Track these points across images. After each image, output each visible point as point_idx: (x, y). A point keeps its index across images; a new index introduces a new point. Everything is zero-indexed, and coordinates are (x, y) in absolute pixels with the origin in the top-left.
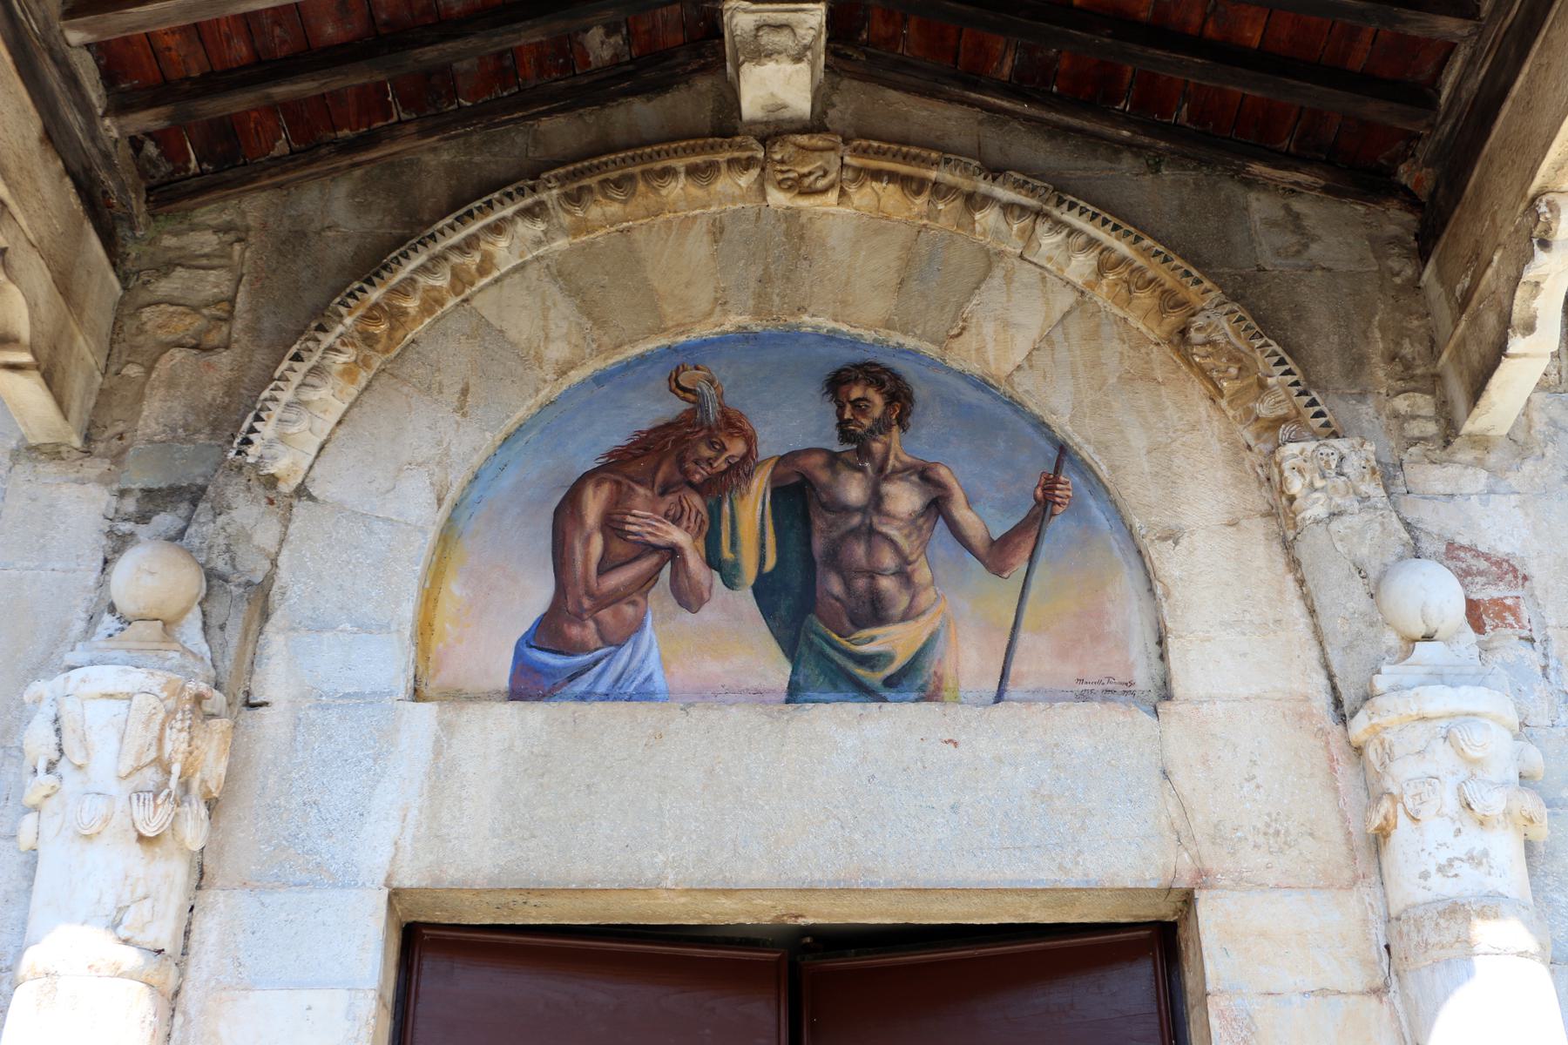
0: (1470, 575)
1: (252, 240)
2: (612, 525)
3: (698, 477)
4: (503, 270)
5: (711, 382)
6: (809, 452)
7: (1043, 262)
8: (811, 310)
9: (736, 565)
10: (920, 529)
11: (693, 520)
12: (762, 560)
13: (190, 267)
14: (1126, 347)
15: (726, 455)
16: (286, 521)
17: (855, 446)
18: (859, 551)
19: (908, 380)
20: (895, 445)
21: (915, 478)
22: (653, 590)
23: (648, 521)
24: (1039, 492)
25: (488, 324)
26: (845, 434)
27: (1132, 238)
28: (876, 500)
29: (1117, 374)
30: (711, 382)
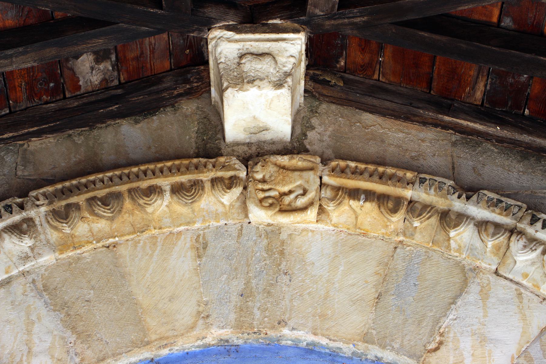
7: (518, 279)
8: (291, 323)
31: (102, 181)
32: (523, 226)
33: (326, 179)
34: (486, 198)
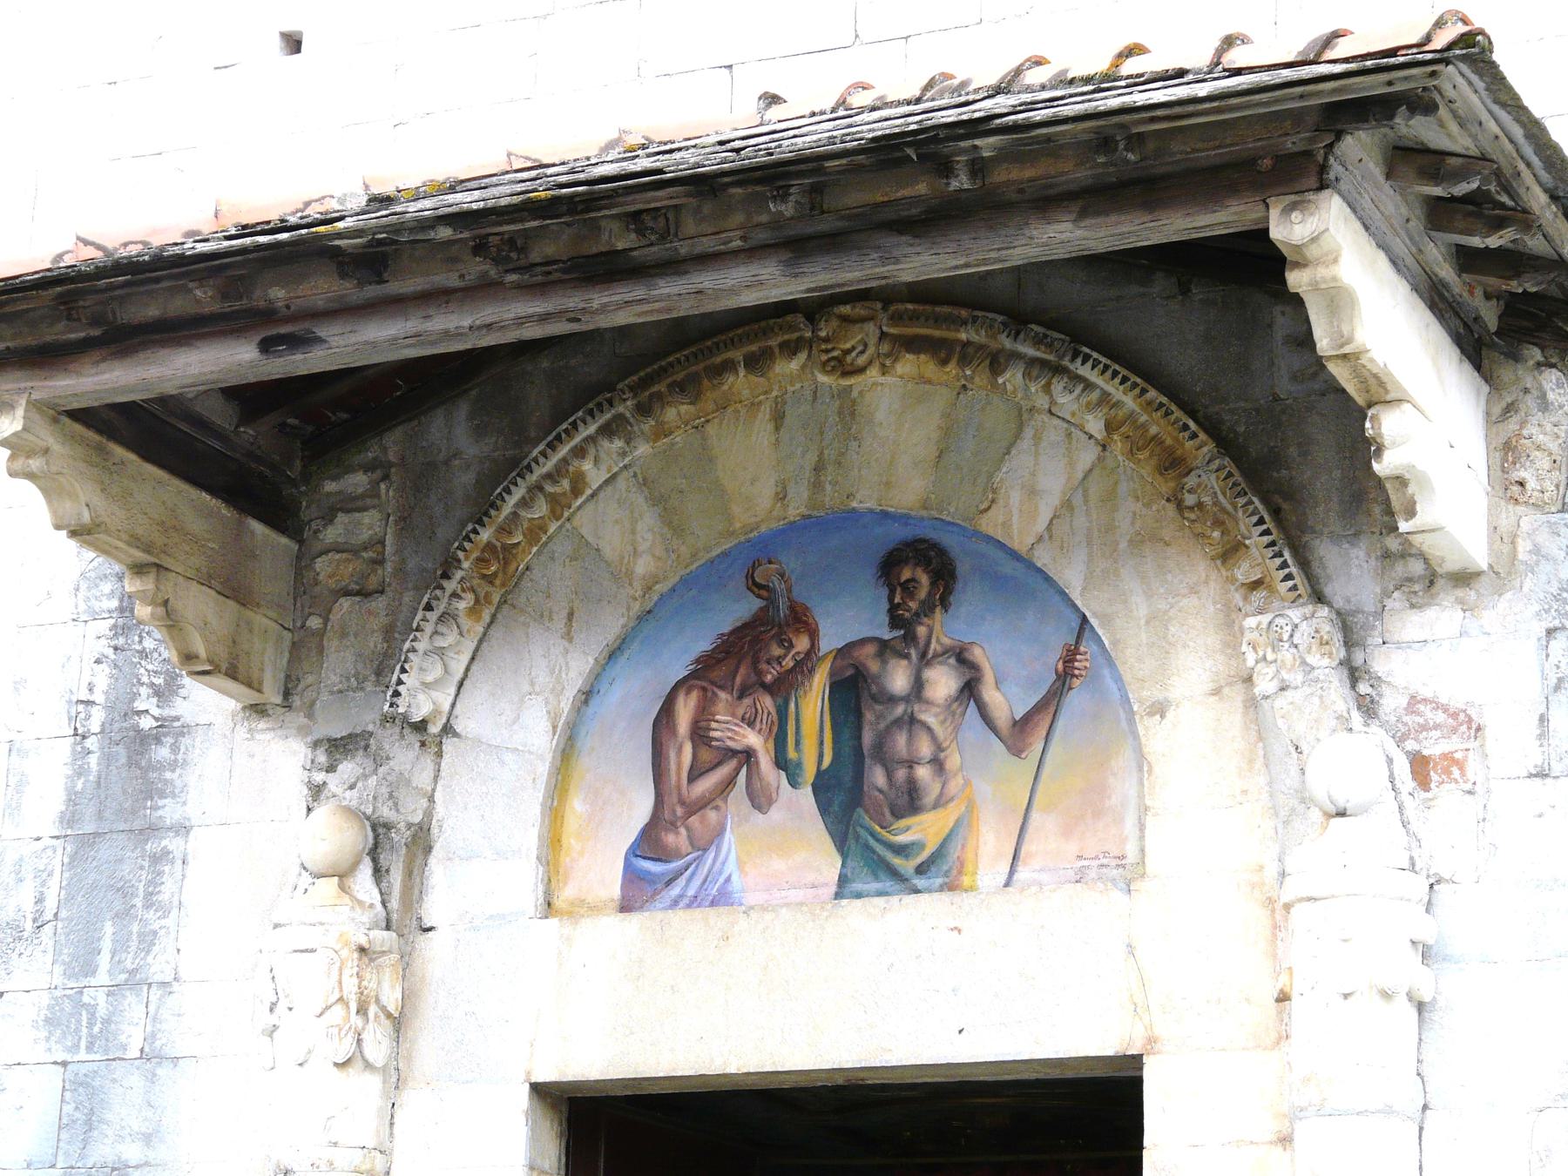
0: (1427, 730)
1: (394, 478)
2: (699, 734)
3: (769, 677)
4: (595, 487)
5: (782, 575)
6: (863, 642)
7: (1068, 417)
8: (858, 497)
9: (799, 765)
10: (953, 714)
11: (764, 722)
12: (821, 756)
13: (348, 511)
14: (1139, 505)
15: (793, 652)
16: (439, 754)
17: (902, 632)
18: (901, 740)
19: (952, 555)
20: (937, 627)
21: (952, 661)
22: (732, 794)
23: (728, 726)
24: (1060, 666)
25: (588, 543)
26: (895, 621)
27: (1137, 391)
28: (918, 685)
29: (1128, 537)
30: (782, 575)
31: (679, 361)
32: (1066, 362)
33: (885, 329)
34: (1033, 334)
